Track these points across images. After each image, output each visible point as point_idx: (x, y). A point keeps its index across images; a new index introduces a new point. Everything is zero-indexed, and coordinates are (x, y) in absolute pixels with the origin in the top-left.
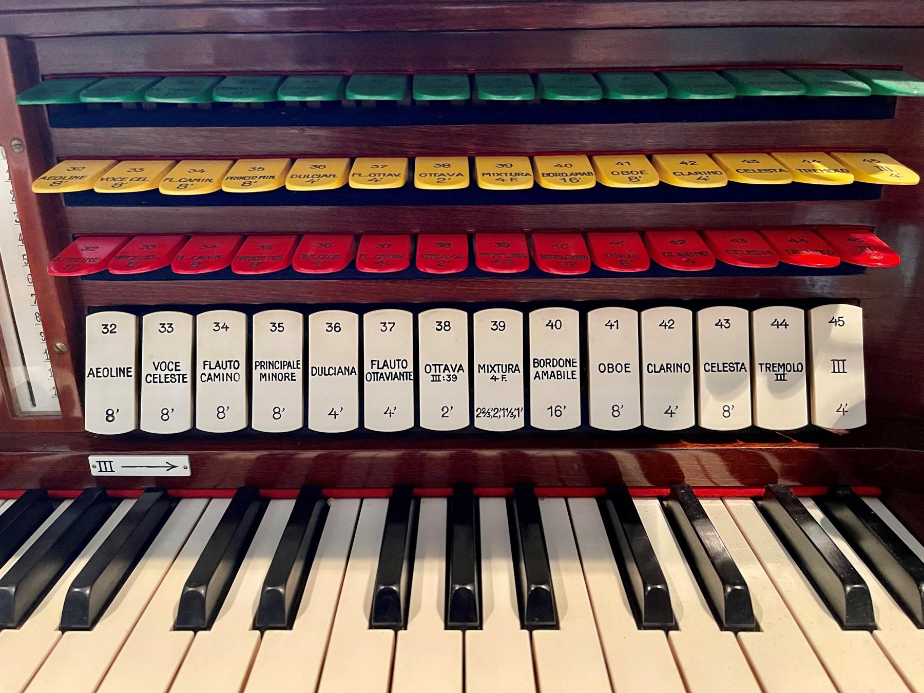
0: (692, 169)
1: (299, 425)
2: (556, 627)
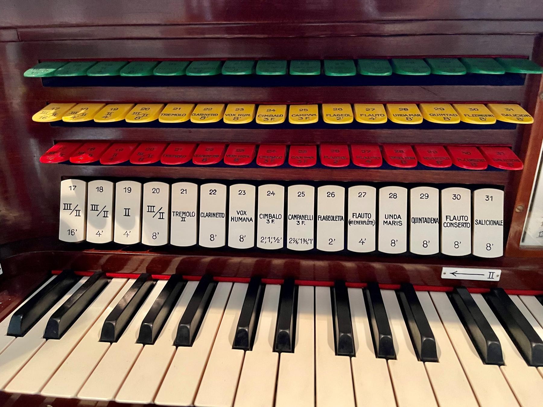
0: (475, 112)
1: (223, 244)
2: (437, 361)
